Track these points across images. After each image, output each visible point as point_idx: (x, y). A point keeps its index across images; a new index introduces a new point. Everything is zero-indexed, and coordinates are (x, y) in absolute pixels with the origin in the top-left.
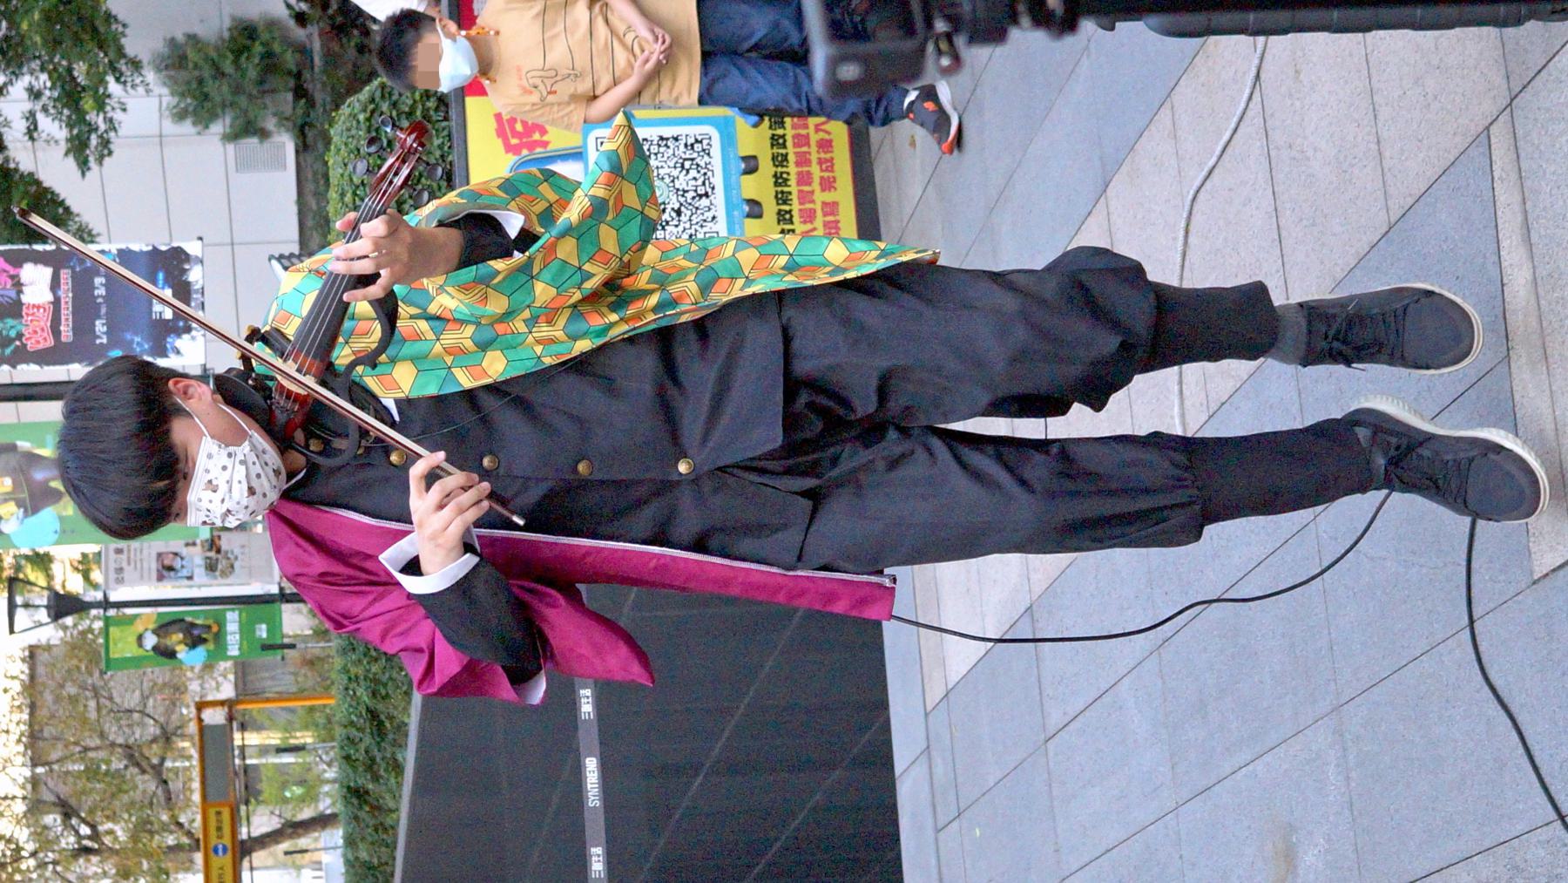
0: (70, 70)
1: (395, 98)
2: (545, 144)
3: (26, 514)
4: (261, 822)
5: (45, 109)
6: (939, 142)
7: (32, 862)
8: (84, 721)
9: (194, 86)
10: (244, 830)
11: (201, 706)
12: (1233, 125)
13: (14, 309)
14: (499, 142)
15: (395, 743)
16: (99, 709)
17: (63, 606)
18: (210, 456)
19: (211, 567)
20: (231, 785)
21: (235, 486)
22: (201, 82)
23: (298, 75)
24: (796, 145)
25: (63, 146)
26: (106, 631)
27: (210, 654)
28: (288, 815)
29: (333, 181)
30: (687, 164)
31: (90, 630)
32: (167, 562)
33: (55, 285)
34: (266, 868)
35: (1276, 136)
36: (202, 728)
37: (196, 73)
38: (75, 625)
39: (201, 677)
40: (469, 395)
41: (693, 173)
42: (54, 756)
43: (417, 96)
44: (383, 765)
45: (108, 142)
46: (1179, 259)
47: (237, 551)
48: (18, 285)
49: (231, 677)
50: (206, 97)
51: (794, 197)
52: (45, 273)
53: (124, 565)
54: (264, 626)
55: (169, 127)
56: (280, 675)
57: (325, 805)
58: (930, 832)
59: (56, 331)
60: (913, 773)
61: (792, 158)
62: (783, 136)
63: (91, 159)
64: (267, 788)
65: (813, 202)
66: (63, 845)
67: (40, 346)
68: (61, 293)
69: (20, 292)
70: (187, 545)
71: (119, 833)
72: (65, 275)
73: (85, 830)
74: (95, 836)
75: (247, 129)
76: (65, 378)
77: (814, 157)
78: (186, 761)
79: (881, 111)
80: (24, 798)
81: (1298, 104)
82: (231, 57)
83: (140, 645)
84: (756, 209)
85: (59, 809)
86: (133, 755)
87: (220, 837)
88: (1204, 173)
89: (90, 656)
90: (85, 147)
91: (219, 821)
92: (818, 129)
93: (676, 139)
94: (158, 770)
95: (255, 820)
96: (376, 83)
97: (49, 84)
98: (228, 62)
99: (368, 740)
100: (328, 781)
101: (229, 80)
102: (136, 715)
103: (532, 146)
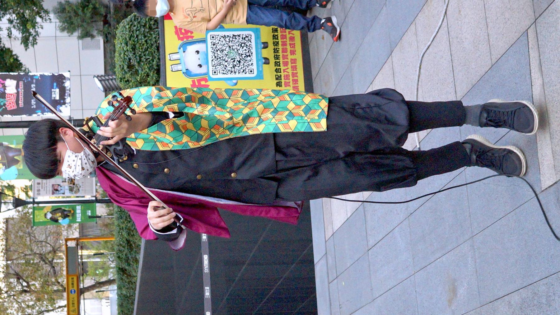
0: (23, 14)
1: (139, 20)
2: (192, 37)
3: (6, 168)
4: (88, 282)
5: (14, 27)
6: (333, 37)
7: (6, 295)
8: (25, 245)
9: (68, 19)
10: (82, 285)
11: (67, 240)
12: (437, 30)
13: (3, 95)
14: (176, 36)
15: (136, 252)
16: (30, 240)
17: (18, 203)
18: (69, 156)
19: (71, 190)
20: (77, 269)
21: (77, 166)
22: (70, 18)
23: (106, 16)
24: (282, 38)
25: (20, 41)
26: (33, 213)
27: (71, 221)
28: (97, 280)
29: (117, 49)
30: (243, 45)
31: (28, 213)
32: (55, 188)
33: (17, 87)
34: (89, 299)
35: (452, 33)
36: (67, 248)
37: (69, 15)
38: (23, 211)
39: (67, 230)
40: (163, 152)
41: (245, 48)
42: (14, 257)
43: (147, 19)
44: (132, 260)
45: (36, 39)
46: (417, 78)
47: (81, 184)
48: (4, 87)
49: (78, 230)
50: (72, 23)
51: (281, 57)
52: (14, 82)
53: (40, 189)
54: (90, 211)
55: (59, 33)
56: (95, 229)
57: (111, 276)
58: (326, 283)
59: (17, 104)
60: (321, 262)
61: (280, 43)
62: (277, 35)
63: (30, 44)
64: (90, 270)
65: (288, 59)
66: (17, 289)
67: (12, 109)
68: (19, 90)
69: (5, 89)
70: (63, 182)
71: (37, 285)
72: (21, 83)
73: (25, 284)
74: (28, 286)
75: (87, 34)
76: (20, 120)
77: (288, 42)
78: (61, 260)
79: (313, 27)
80: (3, 272)
81: (460, 22)
82: (81, 9)
83: (46, 217)
84: (267, 61)
85: (15, 276)
86: (42, 257)
87: (73, 287)
88: (427, 47)
89: (27, 221)
90: (27, 40)
91: (73, 281)
92: (289, 33)
93: (239, 36)
94: (51, 263)
95: (86, 281)
96: (132, 15)
97: (16, 18)
98: (80, 11)
99: (126, 251)
100: (112, 268)
101: (77, 20)
102: (44, 243)
103: (188, 38)
